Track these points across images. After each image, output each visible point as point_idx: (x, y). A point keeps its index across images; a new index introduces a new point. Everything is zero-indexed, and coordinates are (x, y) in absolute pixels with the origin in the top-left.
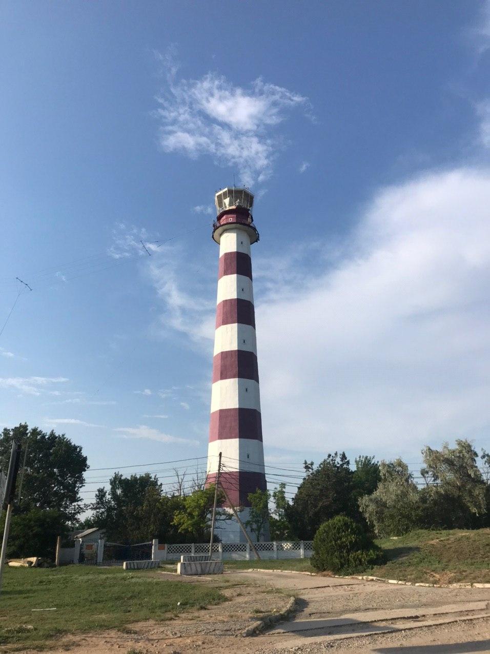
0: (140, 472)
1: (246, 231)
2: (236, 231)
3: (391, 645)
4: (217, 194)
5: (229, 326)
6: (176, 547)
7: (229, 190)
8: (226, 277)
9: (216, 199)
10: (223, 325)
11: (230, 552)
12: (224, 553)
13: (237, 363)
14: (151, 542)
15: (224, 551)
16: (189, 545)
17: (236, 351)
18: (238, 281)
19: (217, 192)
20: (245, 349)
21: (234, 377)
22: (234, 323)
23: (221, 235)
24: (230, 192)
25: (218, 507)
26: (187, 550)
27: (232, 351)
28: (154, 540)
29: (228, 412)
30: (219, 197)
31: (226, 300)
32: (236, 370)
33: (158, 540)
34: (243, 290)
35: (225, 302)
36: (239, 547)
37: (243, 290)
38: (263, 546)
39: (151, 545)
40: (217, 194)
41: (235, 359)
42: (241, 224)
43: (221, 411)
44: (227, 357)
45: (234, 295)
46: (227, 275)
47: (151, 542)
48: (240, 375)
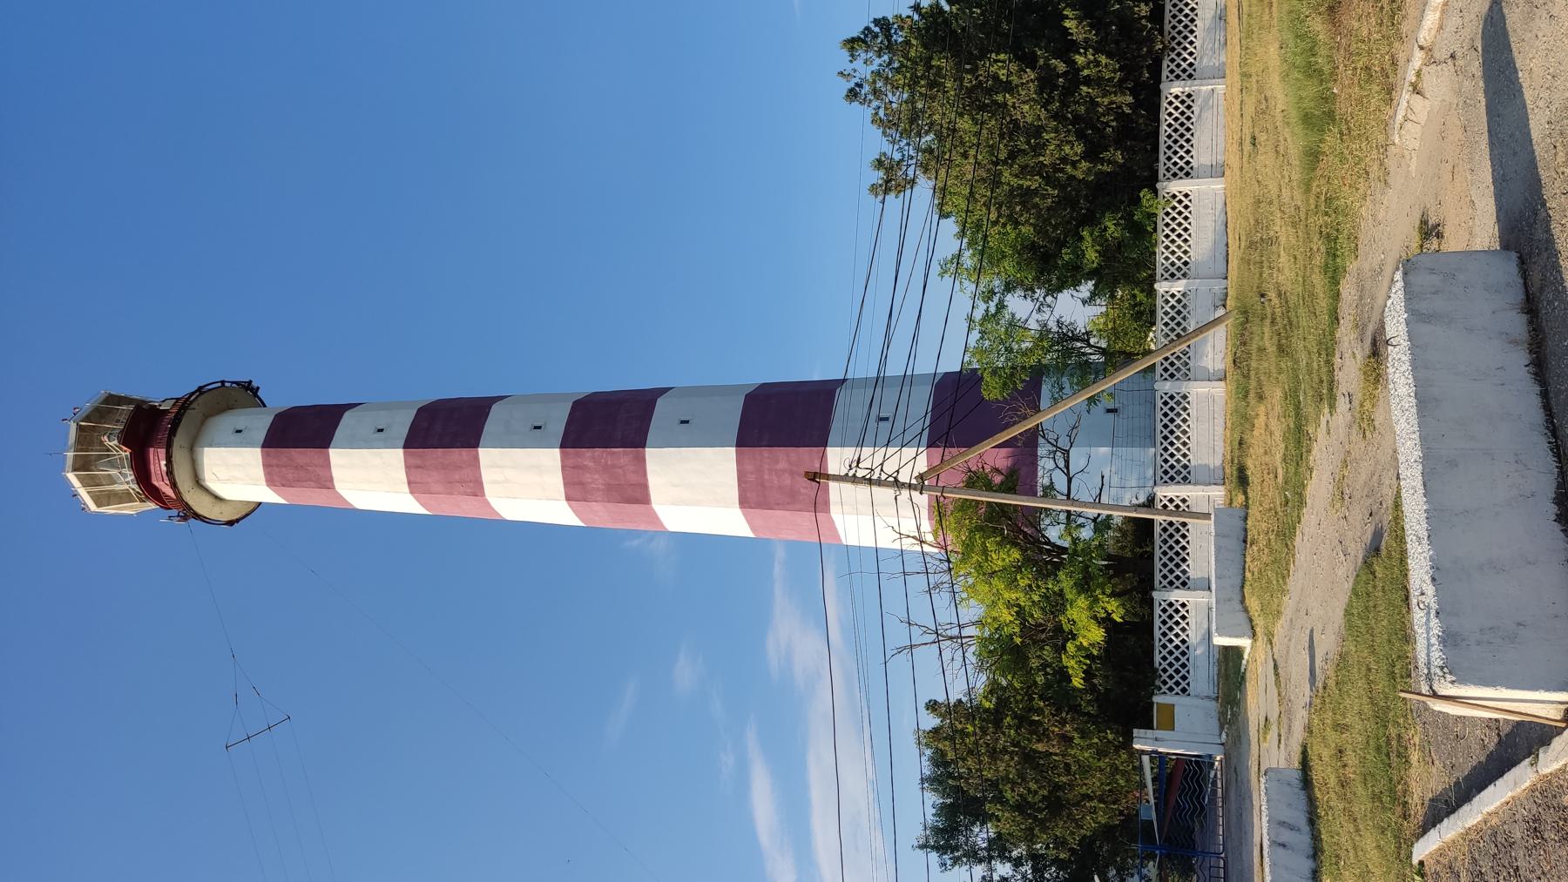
0: (914, 763)
1: (207, 416)
2: (198, 449)
3: (1255, 850)
4: (93, 507)
5: (487, 475)
6: (1165, 553)
7: (75, 470)
8: (336, 487)
9: (110, 510)
10: (483, 494)
11: (1190, 666)
12: (1190, 690)
13: (598, 451)
14: (1146, 759)
15: (1184, 275)
16: (1157, 611)
17: (562, 453)
18: (353, 443)
19: (84, 509)
20: (558, 427)
21: (642, 461)
22: (476, 459)
23: (198, 482)
24: (82, 465)
25: (1037, 493)
26: (1172, 324)
27: (563, 467)
28: (1137, 746)
29: (746, 482)
30: (100, 500)
31: (410, 483)
32: (621, 455)
33: (1135, 731)
34: (381, 430)
35: (414, 486)
36: (1173, 319)
37: (381, 430)
38: (1173, 319)
39: (1159, 759)
40: (93, 507)
41: (589, 457)
42: (173, 432)
43: (744, 503)
44: (581, 484)
45: (394, 458)
46: (331, 479)
47: (1146, 759)
48: (637, 439)
